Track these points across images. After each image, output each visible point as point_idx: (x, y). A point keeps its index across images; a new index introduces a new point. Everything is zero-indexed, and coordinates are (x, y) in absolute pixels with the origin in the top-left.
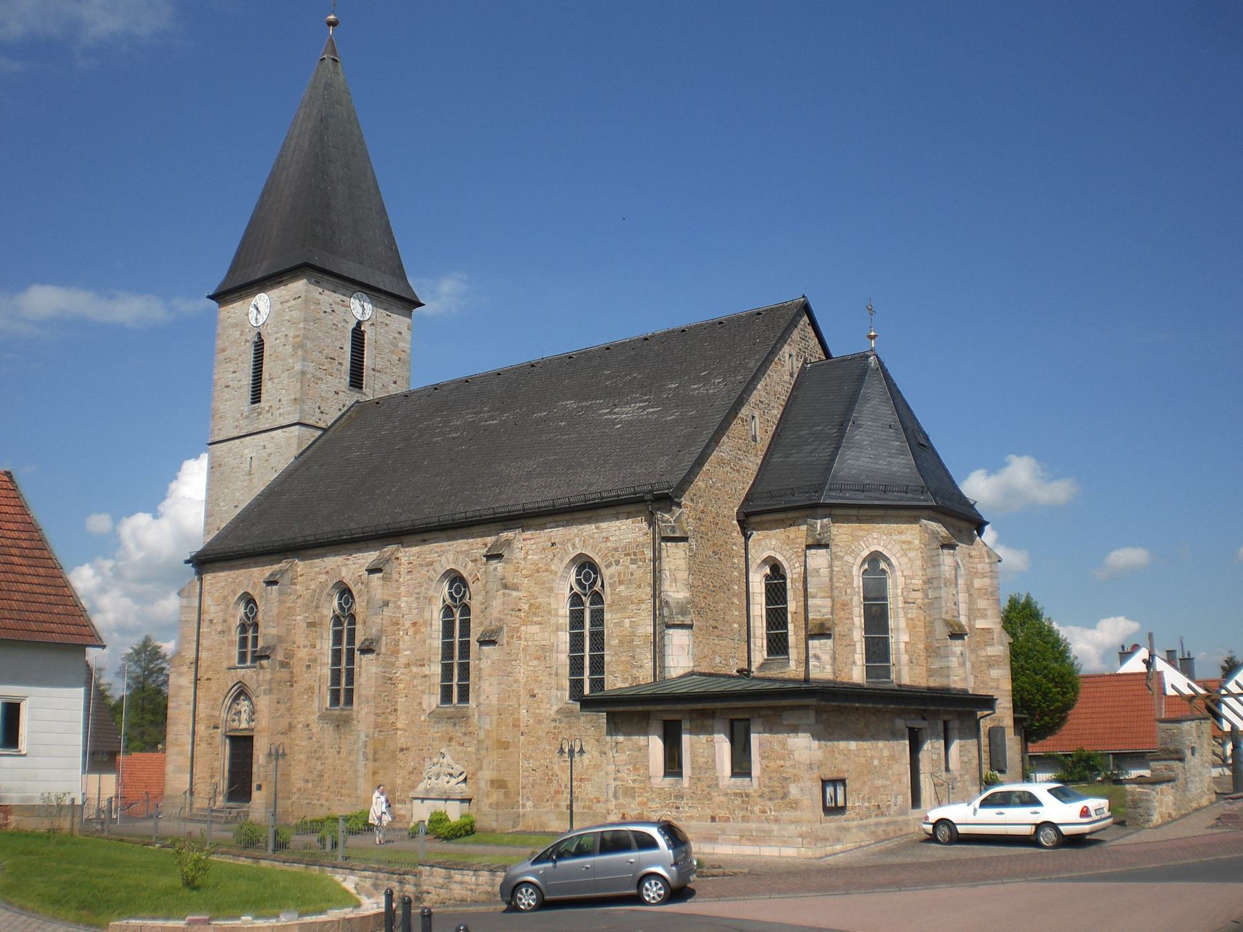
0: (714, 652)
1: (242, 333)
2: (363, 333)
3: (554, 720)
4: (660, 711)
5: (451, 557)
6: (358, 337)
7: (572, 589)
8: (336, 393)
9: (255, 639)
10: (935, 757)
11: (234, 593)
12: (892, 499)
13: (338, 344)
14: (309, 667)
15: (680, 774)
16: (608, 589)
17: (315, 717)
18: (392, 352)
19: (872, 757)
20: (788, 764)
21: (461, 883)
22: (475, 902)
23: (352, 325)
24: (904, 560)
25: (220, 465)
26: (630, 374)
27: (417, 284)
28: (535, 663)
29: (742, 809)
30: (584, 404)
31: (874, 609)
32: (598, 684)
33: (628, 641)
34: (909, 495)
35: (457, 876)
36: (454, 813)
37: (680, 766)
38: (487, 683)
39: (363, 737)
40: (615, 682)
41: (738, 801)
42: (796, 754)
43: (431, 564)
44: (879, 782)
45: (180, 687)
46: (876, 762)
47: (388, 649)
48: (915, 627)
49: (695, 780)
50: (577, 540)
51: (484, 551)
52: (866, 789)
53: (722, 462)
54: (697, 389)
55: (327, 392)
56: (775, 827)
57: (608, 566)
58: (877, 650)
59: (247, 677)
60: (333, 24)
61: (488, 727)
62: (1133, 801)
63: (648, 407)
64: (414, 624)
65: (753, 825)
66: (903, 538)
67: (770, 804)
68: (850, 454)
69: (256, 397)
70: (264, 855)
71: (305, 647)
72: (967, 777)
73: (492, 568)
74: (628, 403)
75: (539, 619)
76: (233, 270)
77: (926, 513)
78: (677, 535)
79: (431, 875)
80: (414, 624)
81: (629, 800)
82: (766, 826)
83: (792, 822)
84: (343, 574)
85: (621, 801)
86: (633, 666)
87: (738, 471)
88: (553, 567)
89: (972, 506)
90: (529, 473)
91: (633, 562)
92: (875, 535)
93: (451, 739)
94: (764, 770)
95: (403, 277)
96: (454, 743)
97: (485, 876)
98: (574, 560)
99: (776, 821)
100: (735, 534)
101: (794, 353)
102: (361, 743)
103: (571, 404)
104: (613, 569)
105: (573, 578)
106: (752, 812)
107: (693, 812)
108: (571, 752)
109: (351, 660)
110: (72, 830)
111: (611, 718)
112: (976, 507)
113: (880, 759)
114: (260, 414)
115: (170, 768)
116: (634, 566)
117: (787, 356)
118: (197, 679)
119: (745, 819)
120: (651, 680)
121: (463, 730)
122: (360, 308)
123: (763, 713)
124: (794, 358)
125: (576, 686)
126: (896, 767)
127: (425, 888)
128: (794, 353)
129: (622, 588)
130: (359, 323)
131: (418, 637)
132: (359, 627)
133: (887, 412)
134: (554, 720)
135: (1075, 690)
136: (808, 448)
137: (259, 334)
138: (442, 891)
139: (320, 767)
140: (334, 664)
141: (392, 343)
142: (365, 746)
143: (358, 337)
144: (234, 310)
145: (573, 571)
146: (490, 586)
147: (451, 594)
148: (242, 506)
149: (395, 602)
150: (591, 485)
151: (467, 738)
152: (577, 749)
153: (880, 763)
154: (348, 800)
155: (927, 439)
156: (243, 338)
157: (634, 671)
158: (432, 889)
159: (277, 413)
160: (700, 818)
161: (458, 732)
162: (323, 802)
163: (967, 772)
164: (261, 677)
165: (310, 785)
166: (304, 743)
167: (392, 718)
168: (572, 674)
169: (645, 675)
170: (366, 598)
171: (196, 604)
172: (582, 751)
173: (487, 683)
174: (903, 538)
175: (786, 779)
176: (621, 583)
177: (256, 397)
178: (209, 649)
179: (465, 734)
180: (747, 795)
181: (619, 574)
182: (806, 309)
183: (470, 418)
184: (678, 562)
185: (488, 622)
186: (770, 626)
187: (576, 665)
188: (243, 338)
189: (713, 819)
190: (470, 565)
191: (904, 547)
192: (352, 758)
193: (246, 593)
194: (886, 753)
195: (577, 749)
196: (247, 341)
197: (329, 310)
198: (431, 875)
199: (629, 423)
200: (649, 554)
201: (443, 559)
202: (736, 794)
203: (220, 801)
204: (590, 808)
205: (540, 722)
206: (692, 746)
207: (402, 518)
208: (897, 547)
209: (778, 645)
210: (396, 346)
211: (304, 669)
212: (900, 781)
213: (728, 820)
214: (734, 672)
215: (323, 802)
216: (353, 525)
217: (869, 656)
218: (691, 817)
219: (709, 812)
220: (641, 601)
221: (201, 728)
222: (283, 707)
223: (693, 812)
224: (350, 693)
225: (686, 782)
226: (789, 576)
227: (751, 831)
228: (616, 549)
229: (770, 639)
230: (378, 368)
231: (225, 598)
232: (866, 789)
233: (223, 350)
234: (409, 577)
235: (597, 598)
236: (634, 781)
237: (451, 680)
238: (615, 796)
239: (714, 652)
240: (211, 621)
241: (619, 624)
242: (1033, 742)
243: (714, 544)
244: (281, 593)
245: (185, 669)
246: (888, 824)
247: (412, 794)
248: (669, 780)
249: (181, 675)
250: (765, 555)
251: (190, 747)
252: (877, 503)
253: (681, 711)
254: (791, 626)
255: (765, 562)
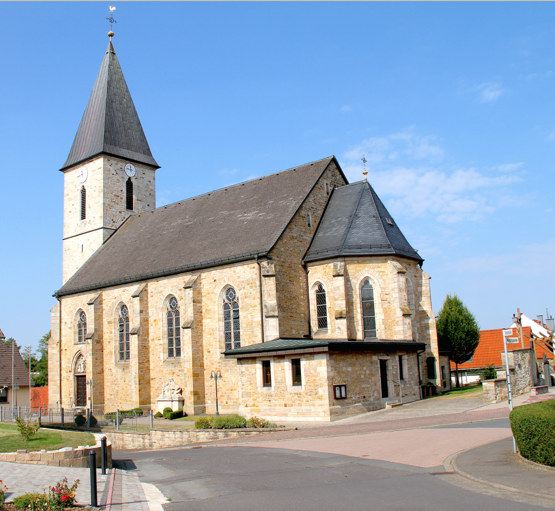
0: (291, 328)
1: (76, 187)
2: (131, 184)
3: (219, 363)
4: (261, 357)
5: (170, 288)
6: (129, 185)
7: (224, 301)
8: (120, 212)
9: (85, 330)
10: (394, 373)
11: (75, 309)
12: (374, 251)
13: (120, 189)
14: (109, 342)
15: (270, 385)
16: (240, 301)
17: (113, 365)
18: (146, 191)
19: (360, 375)
20: (317, 379)
21: (169, 438)
22: (175, 446)
23: (127, 179)
24: (381, 280)
25: (69, 249)
26: (252, 197)
27: (158, 157)
28: (209, 336)
29: (298, 400)
30: (232, 212)
31: (367, 304)
32: (238, 345)
33: (250, 325)
34: (383, 249)
35: (167, 434)
36: (175, 408)
37: (301, 381)
38: (187, 347)
39: (134, 373)
40: (245, 343)
41: (296, 397)
42: (321, 374)
43: (161, 292)
44: (364, 386)
45: (53, 354)
46: (362, 376)
47: (143, 333)
48: (387, 312)
49: (277, 388)
50: (225, 278)
51: (183, 285)
52: (358, 389)
53: (293, 238)
54: (282, 203)
55: (116, 212)
56: (313, 408)
57: (240, 290)
58: (369, 323)
59: (83, 348)
60: (111, 35)
61: (188, 367)
62: (486, 390)
63: (259, 213)
64: (155, 321)
65: (303, 408)
66: (380, 269)
67: (310, 397)
68: (354, 231)
69: (83, 217)
70: (85, 429)
71: (107, 333)
72: (412, 382)
73: (187, 293)
74: (251, 211)
75: (210, 316)
76: (70, 156)
77: (391, 257)
78: (270, 274)
79: (156, 434)
80: (155, 321)
81: (249, 398)
82: (308, 408)
83: (320, 405)
84: (123, 298)
85: (245, 399)
86: (253, 336)
87: (301, 242)
88: (215, 291)
89: (416, 253)
90: (205, 247)
91: (251, 287)
92: (366, 269)
93: (173, 373)
94: (307, 382)
95: (150, 154)
96: (175, 375)
97: (178, 434)
98: (225, 287)
99: (313, 405)
100: (301, 272)
101: (329, 183)
102: (133, 377)
103: (225, 213)
104: (242, 291)
105: (224, 297)
106: (302, 401)
107: (276, 402)
108: (216, 377)
109: (178, 334)
110: (144, 445)
111: (239, 359)
112: (418, 253)
113: (365, 374)
114: (85, 224)
115: (50, 392)
116: (251, 289)
117: (325, 185)
118: (61, 350)
119: (300, 405)
120: (261, 342)
121: (179, 369)
122: (131, 171)
123: (305, 356)
124: (329, 186)
125: (228, 346)
126: (373, 378)
127: (153, 440)
128: (329, 183)
129: (246, 300)
130: (130, 179)
131: (157, 326)
132: (130, 323)
133: (373, 211)
134: (219, 363)
135: (478, 336)
136: (334, 229)
137: (83, 186)
138: (161, 442)
139: (117, 388)
140: (121, 341)
141: (146, 187)
142: (135, 378)
143: (129, 185)
144: (71, 176)
145: (224, 293)
146: (187, 301)
147: (235, 293)
148: (79, 268)
149: (146, 311)
150: (232, 252)
151: (180, 373)
152: (218, 376)
153: (365, 377)
154: (129, 403)
155: (393, 221)
156: (76, 189)
157: (253, 339)
158: (156, 441)
159: (93, 223)
160: (280, 405)
161: (176, 370)
162: (119, 404)
163: (412, 379)
164: (88, 348)
165: (113, 397)
166: (109, 378)
167: (147, 365)
168: (226, 341)
169: (259, 340)
170: (132, 309)
171: (59, 315)
172: (221, 376)
173: (187, 347)
174: (380, 269)
175: (317, 386)
176: (246, 297)
177: (83, 217)
178: (66, 336)
179: (180, 371)
180: (300, 394)
181: (245, 293)
182: (334, 160)
183: (180, 221)
184: (272, 287)
185: (186, 319)
186: (319, 314)
187: (228, 336)
188: (76, 189)
189: (286, 405)
190: (178, 292)
191: (381, 274)
192: (130, 384)
193: (80, 309)
194: (368, 372)
195: (218, 376)
196: (78, 190)
197: (115, 173)
198: (156, 434)
199: (250, 221)
200: (258, 283)
201: (166, 290)
202: (295, 394)
203: (74, 406)
204: (236, 403)
205: (213, 364)
206: (275, 372)
207: (148, 271)
208: (377, 274)
209: (323, 323)
210: (148, 188)
211: (107, 343)
212: (376, 385)
213: (292, 405)
214: (302, 337)
215: (119, 404)
216: (126, 275)
217: (365, 326)
218: (276, 405)
219: (284, 403)
220: (255, 306)
221: (63, 372)
222: (98, 361)
223: (276, 402)
224: (128, 353)
225: (273, 388)
226: (326, 290)
227: (302, 410)
228: (243, 282)
229: (319, 320)
230: (140, 199)
231: (71, 311)
232: (358, 389)
233: (68, 195)
234: (152, 299)
235: (236, 305)
236: (250, 389)
237: (172, 346)
238: (242, 397)
239: (291, 328)
240: (66, 323)
241: (246, 317)
242: (460, 364)
243: (290, 277)
244: (140, 300)
245: (55, 345)
246: (369, 405)
247: (157, 399)
248: (266, 388)
249: (53, 348)
250: (315, 281)
251: (59, 382)
252: (366, 254)
253: (270, 357)
254: (328, 314)
255: (315, 284)
